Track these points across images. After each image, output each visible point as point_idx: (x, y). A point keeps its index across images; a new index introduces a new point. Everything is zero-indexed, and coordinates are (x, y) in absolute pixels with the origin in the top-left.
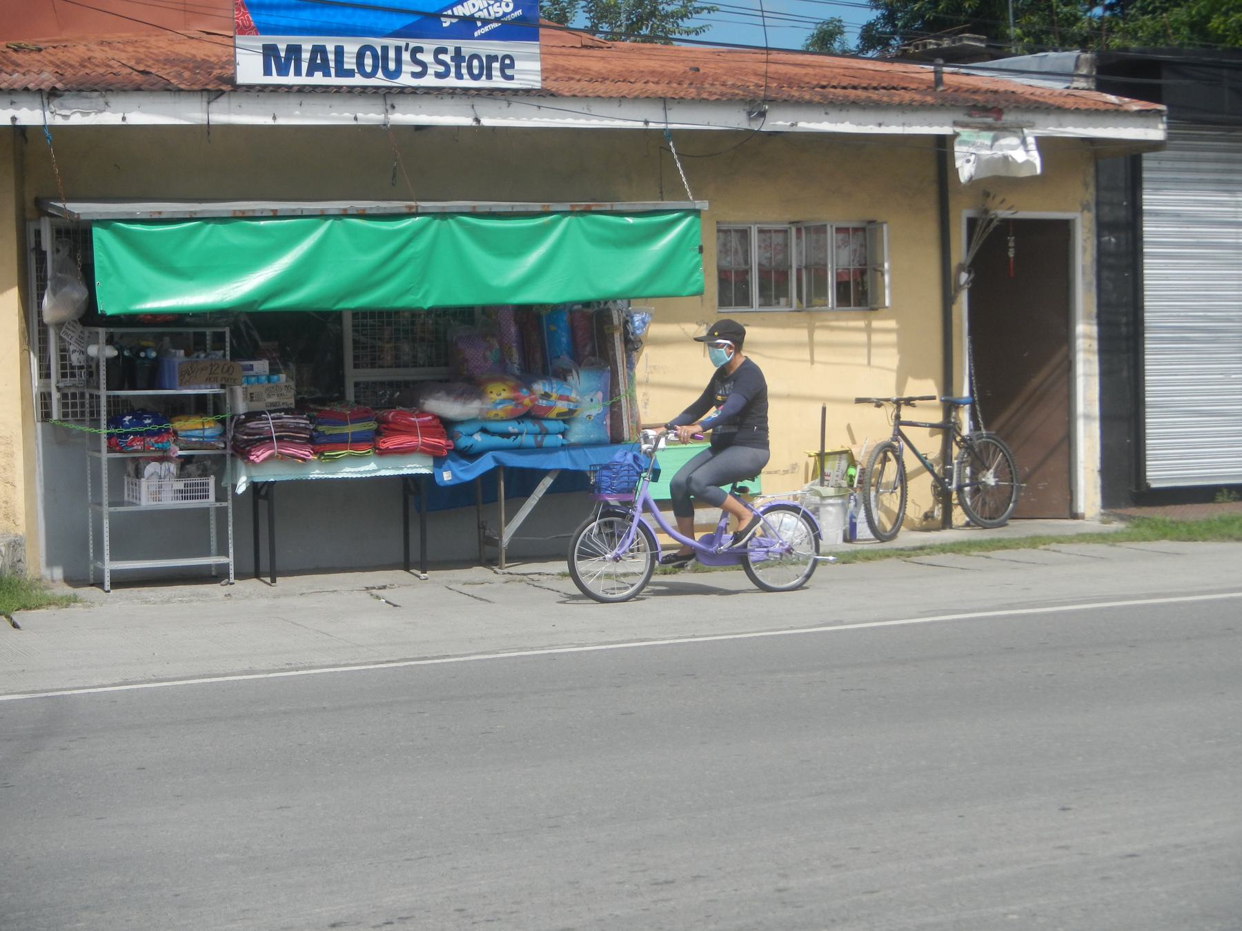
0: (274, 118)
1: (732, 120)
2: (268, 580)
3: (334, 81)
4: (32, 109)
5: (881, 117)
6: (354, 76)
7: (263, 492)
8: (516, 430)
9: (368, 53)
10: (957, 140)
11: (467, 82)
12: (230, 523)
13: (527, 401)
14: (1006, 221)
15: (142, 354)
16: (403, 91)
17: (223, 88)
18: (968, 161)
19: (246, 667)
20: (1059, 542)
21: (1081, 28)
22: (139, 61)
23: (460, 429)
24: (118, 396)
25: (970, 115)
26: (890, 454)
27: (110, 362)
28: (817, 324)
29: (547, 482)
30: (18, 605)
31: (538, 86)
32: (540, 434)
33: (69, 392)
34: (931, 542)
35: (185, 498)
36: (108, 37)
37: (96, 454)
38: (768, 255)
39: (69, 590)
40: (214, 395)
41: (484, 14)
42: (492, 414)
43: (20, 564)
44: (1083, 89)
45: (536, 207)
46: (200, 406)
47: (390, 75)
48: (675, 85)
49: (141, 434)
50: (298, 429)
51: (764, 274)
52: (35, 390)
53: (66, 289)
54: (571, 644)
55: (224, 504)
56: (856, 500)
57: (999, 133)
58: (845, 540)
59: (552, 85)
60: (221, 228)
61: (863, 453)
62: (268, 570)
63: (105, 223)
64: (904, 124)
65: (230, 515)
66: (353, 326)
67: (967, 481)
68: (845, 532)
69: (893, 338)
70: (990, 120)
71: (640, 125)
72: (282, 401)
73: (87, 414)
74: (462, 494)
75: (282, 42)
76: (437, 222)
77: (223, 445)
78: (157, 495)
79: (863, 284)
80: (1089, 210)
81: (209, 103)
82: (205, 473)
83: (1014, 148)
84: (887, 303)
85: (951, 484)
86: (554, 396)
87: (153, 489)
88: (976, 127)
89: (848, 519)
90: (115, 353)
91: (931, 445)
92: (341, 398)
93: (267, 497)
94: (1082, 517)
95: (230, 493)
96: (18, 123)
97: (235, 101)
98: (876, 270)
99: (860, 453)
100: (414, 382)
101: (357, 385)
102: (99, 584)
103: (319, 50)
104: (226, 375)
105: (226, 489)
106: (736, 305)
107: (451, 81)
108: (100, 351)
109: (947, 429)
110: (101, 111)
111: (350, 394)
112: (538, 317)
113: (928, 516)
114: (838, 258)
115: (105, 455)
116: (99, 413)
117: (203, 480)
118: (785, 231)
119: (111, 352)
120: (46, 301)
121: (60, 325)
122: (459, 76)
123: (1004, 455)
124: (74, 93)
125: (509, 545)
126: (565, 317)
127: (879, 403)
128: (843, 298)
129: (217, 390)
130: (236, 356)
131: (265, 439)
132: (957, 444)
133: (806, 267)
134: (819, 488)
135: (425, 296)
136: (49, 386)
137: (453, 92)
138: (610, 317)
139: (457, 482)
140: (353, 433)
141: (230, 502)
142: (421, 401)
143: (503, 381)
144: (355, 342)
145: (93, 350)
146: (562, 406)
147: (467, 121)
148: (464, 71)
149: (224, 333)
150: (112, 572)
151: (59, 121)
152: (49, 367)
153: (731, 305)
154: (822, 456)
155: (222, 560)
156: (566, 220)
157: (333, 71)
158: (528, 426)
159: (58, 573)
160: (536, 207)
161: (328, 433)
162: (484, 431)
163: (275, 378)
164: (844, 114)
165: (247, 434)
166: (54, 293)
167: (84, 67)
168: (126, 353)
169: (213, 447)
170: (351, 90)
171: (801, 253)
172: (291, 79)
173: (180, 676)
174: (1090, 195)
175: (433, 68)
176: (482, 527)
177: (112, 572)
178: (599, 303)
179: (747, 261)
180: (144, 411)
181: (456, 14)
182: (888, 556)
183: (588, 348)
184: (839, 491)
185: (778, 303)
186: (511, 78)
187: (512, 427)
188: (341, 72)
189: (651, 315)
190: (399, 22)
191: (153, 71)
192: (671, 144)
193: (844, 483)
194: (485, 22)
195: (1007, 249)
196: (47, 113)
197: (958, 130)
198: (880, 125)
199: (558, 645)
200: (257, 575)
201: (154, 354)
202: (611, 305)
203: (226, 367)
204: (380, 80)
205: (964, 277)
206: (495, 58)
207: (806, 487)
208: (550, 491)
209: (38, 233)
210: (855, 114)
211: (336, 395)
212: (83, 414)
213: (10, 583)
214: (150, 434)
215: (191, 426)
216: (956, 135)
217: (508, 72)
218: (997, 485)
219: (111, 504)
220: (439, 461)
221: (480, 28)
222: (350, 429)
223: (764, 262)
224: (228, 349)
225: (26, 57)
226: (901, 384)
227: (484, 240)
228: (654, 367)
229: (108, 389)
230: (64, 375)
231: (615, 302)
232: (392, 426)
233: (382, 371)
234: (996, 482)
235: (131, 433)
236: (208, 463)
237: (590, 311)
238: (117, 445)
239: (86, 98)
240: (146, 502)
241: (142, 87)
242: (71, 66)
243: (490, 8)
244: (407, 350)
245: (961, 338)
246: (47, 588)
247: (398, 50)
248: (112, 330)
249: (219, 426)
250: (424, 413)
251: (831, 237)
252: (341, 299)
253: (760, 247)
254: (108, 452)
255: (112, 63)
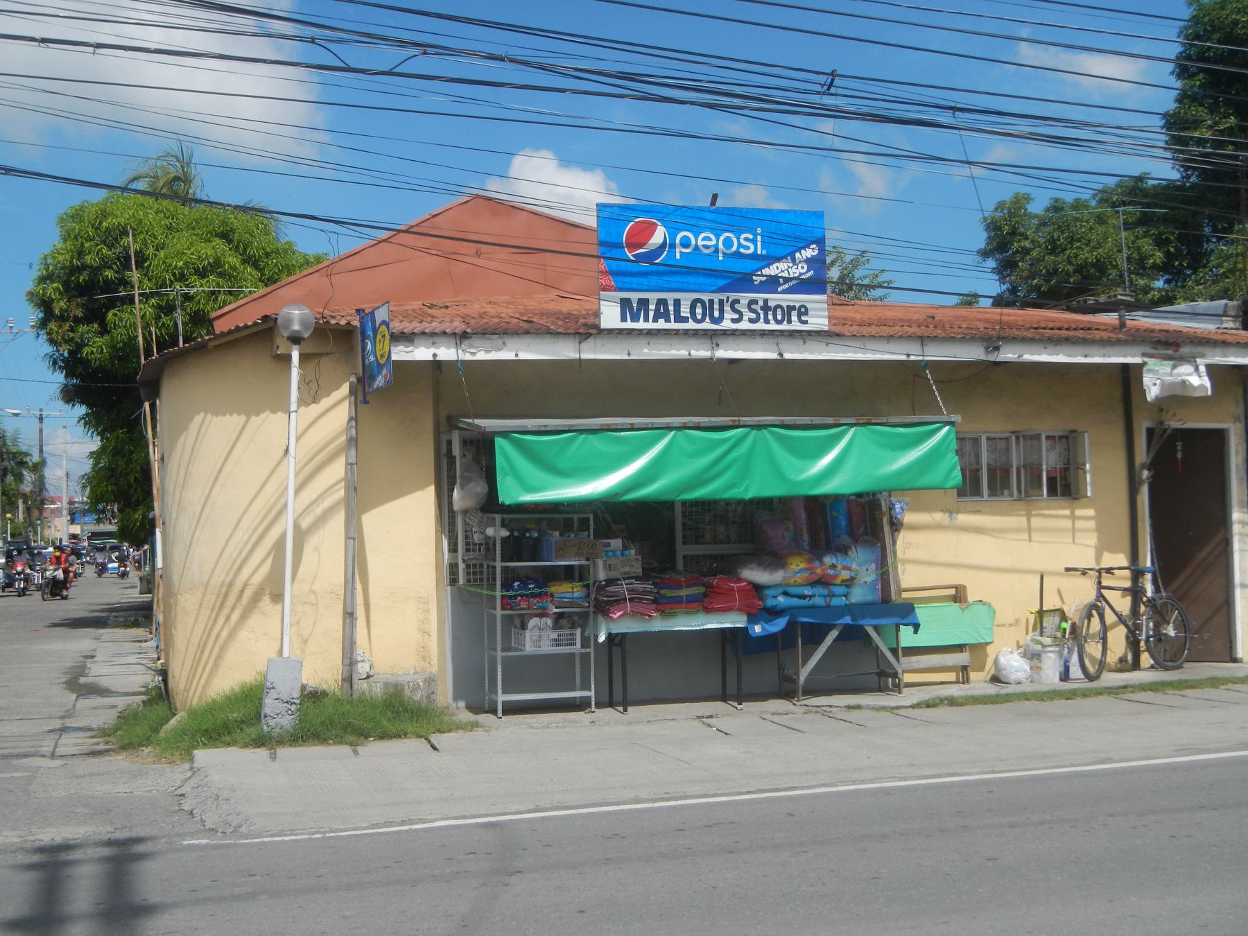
0: (629, 354)
1: (973, 353)
2: (621, 709)
3: (673, 325)
4: (449, 348)
5: (1086, 350)
6: (688, 322)
7: (617, 640)
8: (810, 593)
9: (699, 304)
10: (1145, 369)
11: (773, 326)
12: (593, 669)
13: (819, 571)
14: (1176, 431)
15: (527, 535)
16: (725, 333)
17: (591, 331)
18: (1155, 384)
19: (633, 796)
20: (1235, 683)
21: (1154, 295)
22: (522, 314)
23: (768, 592)
24: (507, 567)
25: (1155, 348)
26: (1094, 612)
27: (504, 540)
28: (1034, 512)
29: (834, 634)
30: (434, 729)
31: (826, 328)
32: (828, 596)
33: (471, 563)
34: (1132, 682)
35: (558, 645)
36: (493, 299)
37: (492, 611)
38: (994, 457)
39: (471, 717)
40: (581, 566)
41: (785, 274)
42: (792, 581)
43: (434, 696)
44: (1232, 329)
45: (830, 420)
46: (569, 574)
47: (715, 321)
48: (923, 328)
49: (526, 596)
50: (646, 592)
51: (992, 472)
52: (446, 562)
53: (472, 485)
54: (893, 777)
55: (588, 650)
56: (1069, 648)
57: (1178, 363)
58: (1061, 680)
59: (837, 329)
60: (591, 437)
61: (1072, 611)
62: (621, 700)
63: (505, 434)
64: (1104, 356)
65: (592, 658)
66: (683, 512)
67: (1151, 633)
68: (1060, 673)
69: (1091, 524)
70: (1170, 352)
71: (904, 358)
72: (632, 571)
73: (485, 580)
74: (768, 642)
75: (634, 296)
76: (754, 432)
77: (587, 605)
78: (537, 643)
79: (1066, 479)
80: (1240, 422)
81: (580, 343)
82: (573, 626)
83: (1190, 375)
84: (1089, 494)
85: (1140, 635)
86: (839, 566)
87: (534, 638)
88: (1159, 358)
89: (1062, 663)
90: (508, 534)
91: (1123, 604)
92: (673, 567)
93: (620, 644)
94: (1240, 661)
95: (592, 641)
96: (438, 359)
97: (599, 341)
98: (1078, 468)
99: (1070, 611)
100: (728, 556)
101: (685, 557)
102: (493, 711)
103: (662, 302)
104: (591, 551)
105: (589, 637)
106: (971, 495)
107: (761, 326)
108: (496, 532)
109: (1135, 592)
110: (500, 350)
111: (680, 565)
112: (823, 506)
113: (1122, 660)
114: (1049, 460)
115: (499, 612)
116: (494, 579)
117: (572, 631)
118: (1007, 439)
119: (505, 533)
120: (456, 494)
121: (465, 512)
122: (767, 321)
123: (1179, 612)
124: (480, 336)
125: (805, 682)
126: (844, 505)
127: (1084, 572)
128: (1052, 491)
129: (583, 562)
130: (596, 536)
131: (619, 600)
132: (1144, 603)
133: (1024, 466)
134: (1039, 638)
135: (746, 490)
136: (457, 558)
137: (763, 333)
138: (879, 506)
139: (766, 633)
140: (687, 596)
141: (592, 648)
142: (739, 571)
143: (800, 554)
144: (684, 525)
145: (490, 532)
146: (845, 575)
147: (773, 355)
148: (770, 317)
149: (589, 518)
150: (503, 702)
151: (468, 357)
152: (456, 544)
153: (966, 496)
154: (1041, 613)
155: (586, 693)
156: (853, 430)
157: (672, 317)
158: (819, 590)
159: (462, 704)
160: (830, 420)
161: (668, 595)
162: (786, 594)
163: (627, 552)
164: (1058, 348)
165: (607, 596)
166: (462, 487)
167: (483, 318)
168: (516, 534)
169: (579, 606)
170: (686, 333)
171: (1019, 455)
172: (641, 325)
173: (581, 803)
174: (1240, 410)
175: (748, 315)
176: (781, 668)
177: (503, 702)
178: (868, 494)
179: (978, 462)
180: (528, 578)
181: (764, 273)
182: (1101, 694)
183: (862, 529)
184: (1055, 641)
185: (1002, 494)
186: (806, 322)
187: (807, 591)
188: (679, 319)
189: (907, 504)
190: (721, 283)
191: (535, 320)
192: (928, 372)
193: (1059, 635)
194: (787, 280)
195: (1176, 451)
196: (460, 351)
197: (1146, 359)
198: (1086, 356)
199: (882, 778)
200: (611, 704)
201: (536, 535)
202: (879, 496)
203: (590, 545)
204: (707, 325)
205: (1145, 474)
206: (793, 308)
207: (1029, 637)
208: (836, 640)
209: (449, 443)
210: (1066, 348)
211: (669, 565)
212: (481, 580)
213: (427, 712)
214: (534, 596)
215: (567, 591)
216: (1144, 364)
217: (803, 318)
218: (1176, 636)
219: (504, 650)
220: (753, 619)
221: (782, 285)
222: (684, 592)
223: (991, 463)
224: (592, 530)
225: (439, 311)
226: (1098, 557)
227: (785, 443)
228: (910, 544)
229: (502, 561)
230: (468, 550)
231: (881, 493)
232: (716, 590)
233: (703, 547)
234: (1176, 633)
235: (520, 595)
236: (576, 618)
237: (863, 500)
238: (509, 604)
239: (489, 339)
240: (529, 649)
241: (531, 331)
242: (473, 318)
243: (790, 270)
244: (723, 531)
245: (1144, 521)
246: (453, 715)
247: (721, 302)
248: (505, 516)
249: (585, 590)
250: (740, 580)
251: (1044, 443)
252: (681, 493)
253: (987, 451)
254: (502, 610)
255: (503, 315)
